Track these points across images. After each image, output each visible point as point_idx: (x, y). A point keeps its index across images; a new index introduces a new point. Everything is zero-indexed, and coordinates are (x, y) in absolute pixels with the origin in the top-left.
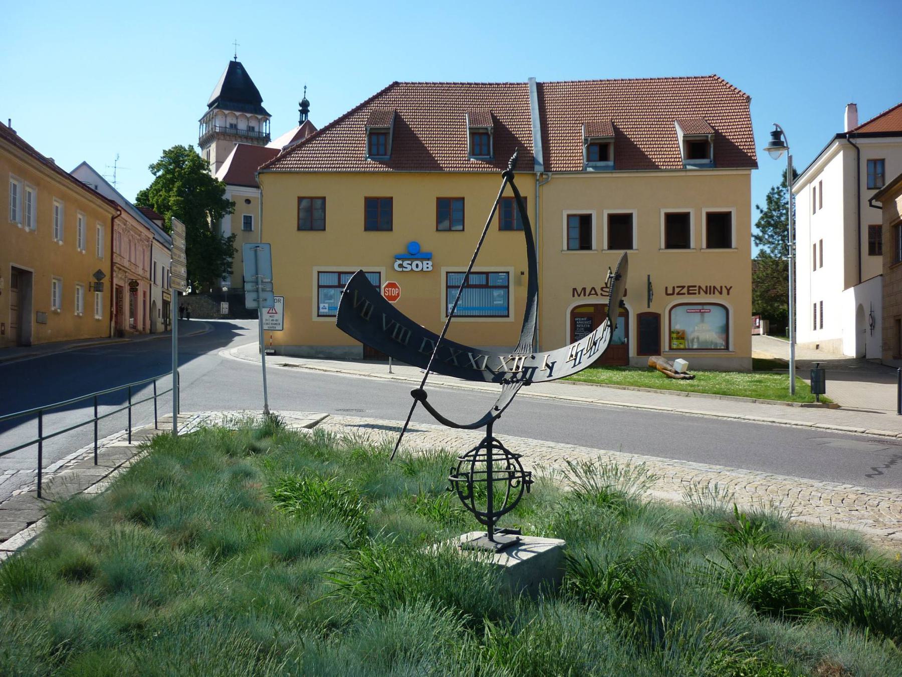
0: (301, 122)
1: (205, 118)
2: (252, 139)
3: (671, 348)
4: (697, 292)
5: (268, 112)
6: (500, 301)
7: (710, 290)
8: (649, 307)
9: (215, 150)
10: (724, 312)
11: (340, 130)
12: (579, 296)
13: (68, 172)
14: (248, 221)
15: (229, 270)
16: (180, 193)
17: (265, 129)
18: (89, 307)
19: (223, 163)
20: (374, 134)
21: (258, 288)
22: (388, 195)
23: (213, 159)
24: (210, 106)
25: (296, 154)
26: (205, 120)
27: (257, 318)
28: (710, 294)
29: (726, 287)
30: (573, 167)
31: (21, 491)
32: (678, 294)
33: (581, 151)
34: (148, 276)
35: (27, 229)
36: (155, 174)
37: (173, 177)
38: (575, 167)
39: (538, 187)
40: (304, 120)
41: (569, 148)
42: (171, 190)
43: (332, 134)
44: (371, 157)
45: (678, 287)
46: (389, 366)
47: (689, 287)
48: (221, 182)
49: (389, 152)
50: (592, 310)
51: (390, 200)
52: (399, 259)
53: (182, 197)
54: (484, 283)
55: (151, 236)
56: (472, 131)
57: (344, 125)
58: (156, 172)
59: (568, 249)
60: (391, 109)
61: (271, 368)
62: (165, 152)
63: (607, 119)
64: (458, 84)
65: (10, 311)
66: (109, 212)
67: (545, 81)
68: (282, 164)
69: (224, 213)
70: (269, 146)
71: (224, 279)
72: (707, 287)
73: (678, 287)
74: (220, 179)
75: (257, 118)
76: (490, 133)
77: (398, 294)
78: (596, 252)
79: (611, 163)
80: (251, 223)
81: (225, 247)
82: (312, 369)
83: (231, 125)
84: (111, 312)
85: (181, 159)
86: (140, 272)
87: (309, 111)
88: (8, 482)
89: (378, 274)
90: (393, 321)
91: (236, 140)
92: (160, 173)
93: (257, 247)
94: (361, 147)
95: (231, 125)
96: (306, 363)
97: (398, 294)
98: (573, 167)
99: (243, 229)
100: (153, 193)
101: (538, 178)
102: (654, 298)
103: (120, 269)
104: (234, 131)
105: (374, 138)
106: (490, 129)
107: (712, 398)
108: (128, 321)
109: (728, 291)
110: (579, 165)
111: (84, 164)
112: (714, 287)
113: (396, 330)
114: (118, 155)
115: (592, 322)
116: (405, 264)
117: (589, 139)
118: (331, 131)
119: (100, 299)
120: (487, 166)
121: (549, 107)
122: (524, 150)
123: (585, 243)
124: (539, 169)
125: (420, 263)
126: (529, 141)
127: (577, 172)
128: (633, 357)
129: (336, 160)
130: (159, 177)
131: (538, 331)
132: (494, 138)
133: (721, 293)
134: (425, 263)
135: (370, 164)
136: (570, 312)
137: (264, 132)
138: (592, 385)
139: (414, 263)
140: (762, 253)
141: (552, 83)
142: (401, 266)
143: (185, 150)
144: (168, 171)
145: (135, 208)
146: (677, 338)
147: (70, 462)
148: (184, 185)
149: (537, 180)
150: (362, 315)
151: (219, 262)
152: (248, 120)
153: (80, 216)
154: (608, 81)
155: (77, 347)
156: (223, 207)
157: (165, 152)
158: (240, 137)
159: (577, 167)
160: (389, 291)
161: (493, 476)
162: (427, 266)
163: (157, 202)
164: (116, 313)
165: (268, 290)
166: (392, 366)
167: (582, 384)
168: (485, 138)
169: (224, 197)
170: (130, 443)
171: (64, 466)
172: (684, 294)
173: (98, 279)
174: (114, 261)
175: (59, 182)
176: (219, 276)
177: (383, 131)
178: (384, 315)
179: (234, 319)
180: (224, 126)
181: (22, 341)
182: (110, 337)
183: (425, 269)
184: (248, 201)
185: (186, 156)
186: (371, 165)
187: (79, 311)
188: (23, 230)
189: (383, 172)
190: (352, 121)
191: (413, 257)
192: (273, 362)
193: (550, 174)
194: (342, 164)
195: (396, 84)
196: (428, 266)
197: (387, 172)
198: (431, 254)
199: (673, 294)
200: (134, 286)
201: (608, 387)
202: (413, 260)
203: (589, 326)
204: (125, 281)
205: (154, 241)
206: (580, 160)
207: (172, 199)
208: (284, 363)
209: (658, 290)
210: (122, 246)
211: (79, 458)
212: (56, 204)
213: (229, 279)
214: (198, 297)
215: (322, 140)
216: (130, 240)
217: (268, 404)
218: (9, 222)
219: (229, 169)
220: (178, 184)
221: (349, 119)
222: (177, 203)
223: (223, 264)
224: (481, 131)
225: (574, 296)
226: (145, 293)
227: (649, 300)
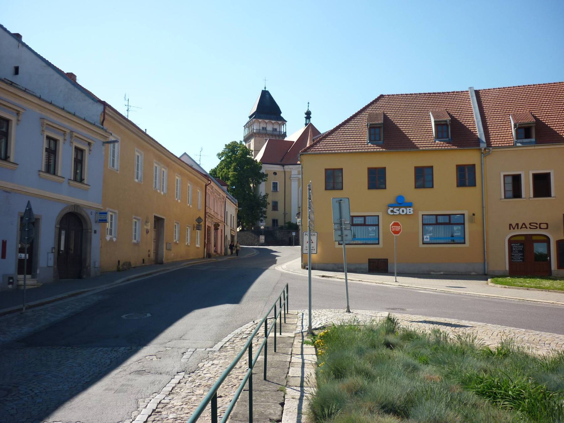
0: (306, 124)
1: (247, 125)
2: (275, 136)
5: (285, 119)
9: (253, 143)
11: (349, 126)
12: (514, 229)
14: (275, 185)
15: (264, 215)
16: (235, 170)
17: (283, 129)
18: (193, 239)
19: (259, 151)
20: (372, 128)
21: (342, 228)
22: (383, 166)
23: (252, 148)
24: (250, 117)
25: (323, 142)
26: (248, 126)
27: (297, 244)
30: (506, 143)
31: (203, 364)
33: (511, 133)
34: (224, 221)
35: (162, 193)
36: (220, 159)
37: (230, 160)
38: (508, 143)
39: (483, 157)
40: (308, 123)
41: (502, 131)
42: (230, 168)
43: (344, 128)
44: (371, 142)
46: (394, 277)
48: (259, 162)
49: (382, 139)
50: (523, 238)
51: (383, 170)
52: (391, 207)
53: (236, 172)
54: (363, 223)
55: (225, 196)
56: (437, 123)
57: (351, 123)
58: (221, 158)
59: (505, 198)
60: (381, 111)
61: (314, 278)
62: (226, 145)
63: (527, 111)
64: (422, 94)
65: (153, 242)
66: (204, 182)
67: (480, 89)
68: (314, 149)
69: (261, 181)
70: (286, 139)
71: (262, 221)
74: (258, 161)
75: (278, 123)
76: (448, 123)
77: (400, 230)
78: (525, 199)
79: (533, 140)
80: (277, 187)
81: (262, 202)
82: (342, 279)
83: (263, 128)
84: (205, 242)
85: (236, 149)
86: (220, 218)
87: (311, 117)
88: (192, 357)
89: (463, 215)
91: (266, 137)
92: (223, 158)
93: (340, 200)
94: (364, 136)
95: (263, 128)
96: (336, 275)
97: (400, 230)
98: (506, 143)
100: (219, 170)
101: (483, 151)
103: (209, 216)
104: (264, 132)
105: (372, 130)
106: (448, 121)
108: (213, 249)
110: (510, 142)
114: (202, 148)
115: (523, 247)
116: (395, 210)
117: (518, 124)
118: (343, 127)
119: (199, 234)
120: (448, 145)
121: (485, 105)
122: (471, 134)
123: (517, 193)
124: (483, 146)
125: (404, 209)
126: (474, 128)
127: (509, 147)
128: (555, 270)
129: (348, 145)
130: (223, 160)
131: (486, 253)
132: (451, 127)
134: (408, 209)
135: (370, 147)
136: (507, 240)
137: (283, 131)
138: (542, 291)
139: (401, 209)
141: (485, 90)
142: (392, 211)
143: (238, 144)
144: (228, 157)
147: (226, 343)
148: (237, 165)
149: (482, 153)
151: (259, 211)
152: (273, 125)
153: (189, 185)
154: (484, 90)
155: (189, 264)
156: (260, 177)
157: (226, 145)
158: (268, 135)
159: (510, 143)
160: (394, 228)
162: (410, 211)
163: (222, 175)
164: (207, 244)
165: (348, 229)
166: (397, 277)
167: (534, 290)
168: (445, 127)
169: (261, 171)
170: (281, 334)
171: (223, 347)
173: (198, 223)
174: (207, 211)
175: (180, 165)
176: (258, 219)
177: (378, 126)
179: (269, 246)
180: (259, 129)
181: (158, 262)
182: (204, 258)
183: (408, 213)
184: (275, 173)
185: (238, 147)
186: (372, 147)
187: (188, 242)
188: (160, 193)
189: (379, 152)
190: (356, 120)
191: (400, 205)
192: (315, 274)
193: (491, 148)
194: (323, 148)
195: (382, 96)
196: (410, 211)
197: (382, 151)
198: (411, 203)
200: (216, 226)
201: (555, 292)
202: (400, 207)
203: (521, 249)
204: (212, 223)
205: (227, 199)
206: (511, 138)
207: (231, 173)
208: (322, 275)
210: (210, 202)
211: (230, 341)
212: (177, 178)
213: (264, 221)
214: (246, 233)
215: (338, 133)
216: (214, 199)
217: (349, 305)
218: (153, 189)
219: (264, 154)
220: (234, 164)
221: (354, 119)
222: (234, 176)
223: (261, 212)
224: (443, 123)
225: (510, 229)
226: (222, 230)
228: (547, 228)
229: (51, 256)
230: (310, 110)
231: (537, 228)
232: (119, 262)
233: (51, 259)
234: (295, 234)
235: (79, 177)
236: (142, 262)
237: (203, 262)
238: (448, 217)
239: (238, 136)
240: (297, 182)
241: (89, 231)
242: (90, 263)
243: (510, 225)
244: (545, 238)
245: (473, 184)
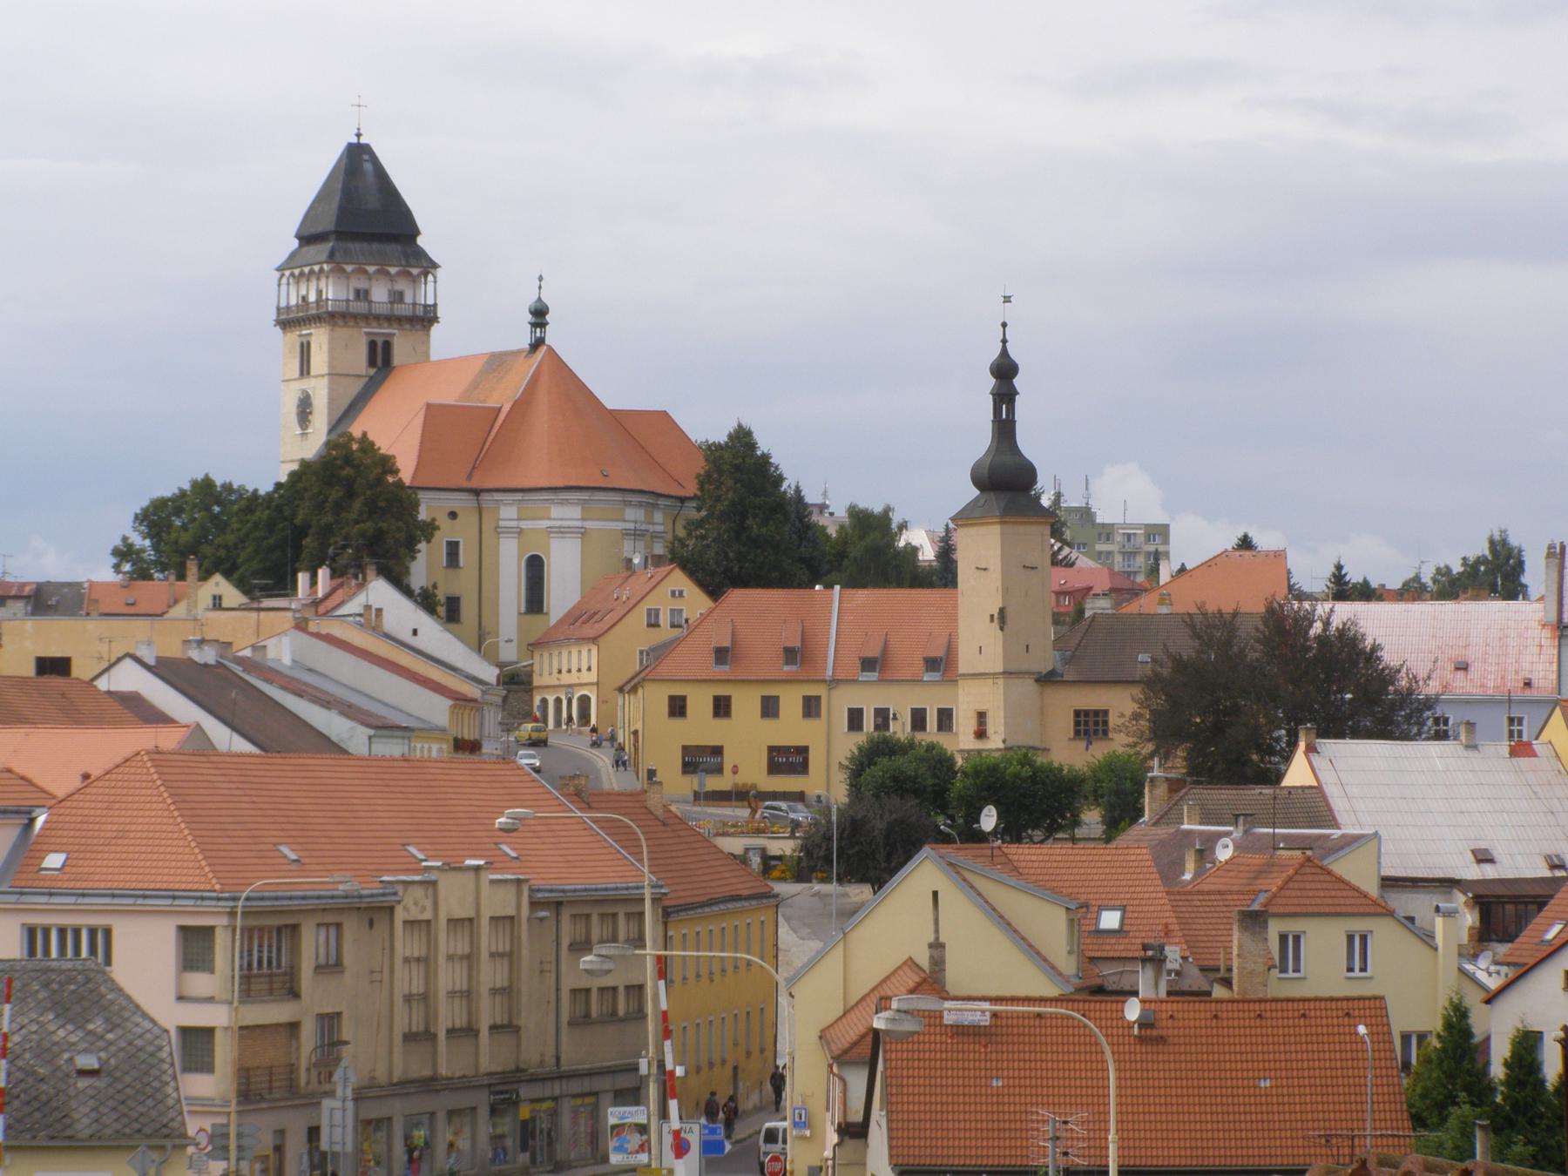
6: (418, 988)
99: (445, 564)
145: (1403, 920)
158: (377, 318)
161: (643, 514)
236: (375, 922)
237: (273, 906)
239: (400, 475)
240: (516, 540)
245: (818, 715)
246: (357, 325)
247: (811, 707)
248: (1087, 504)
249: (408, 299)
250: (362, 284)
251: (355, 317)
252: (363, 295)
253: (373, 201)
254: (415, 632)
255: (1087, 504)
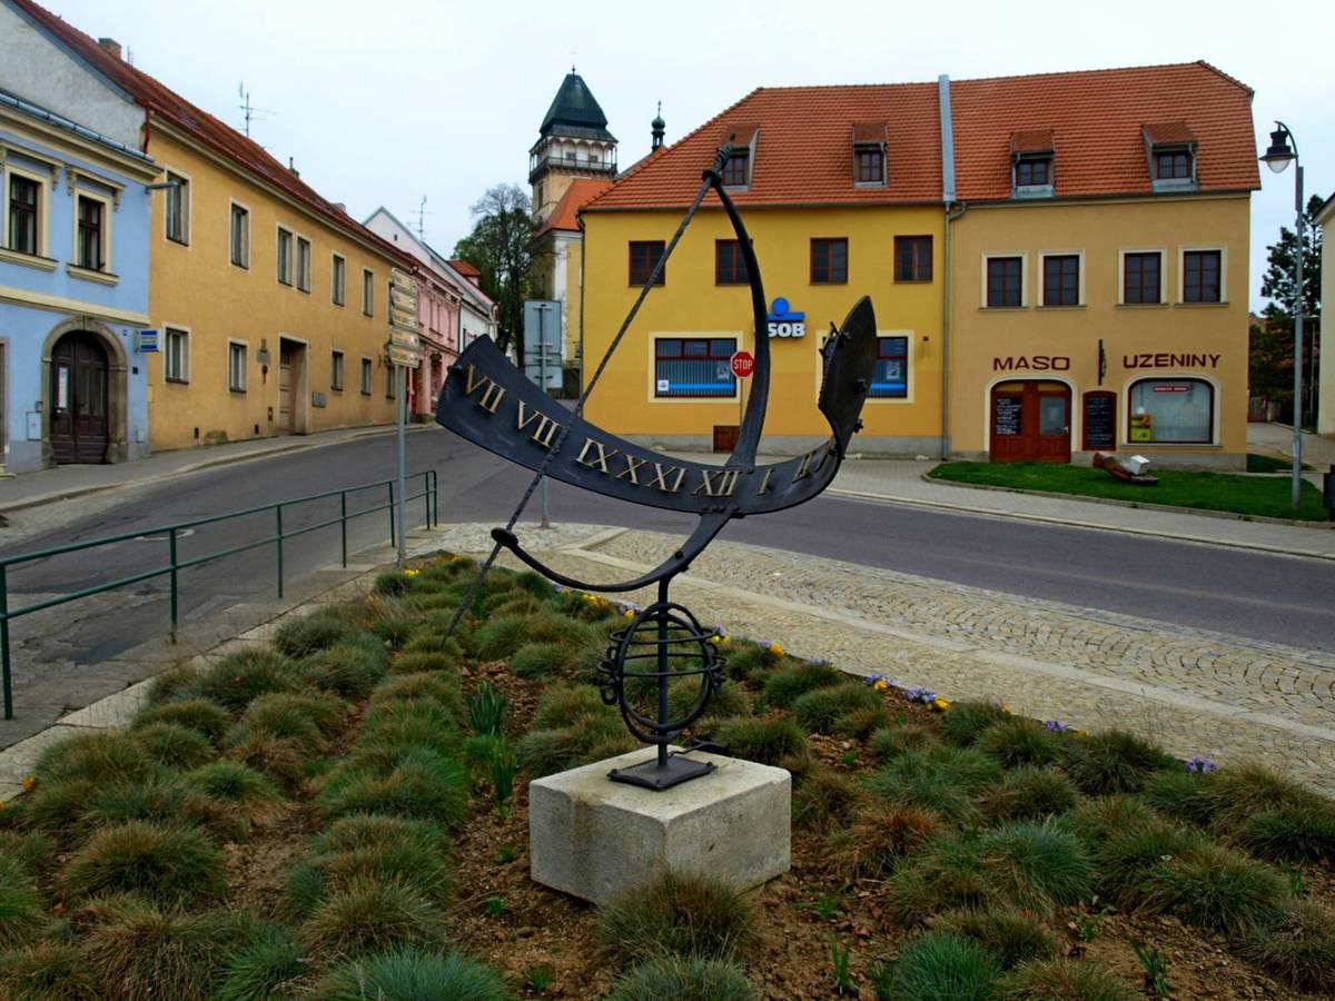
3: (1129, 441)
4: (1169, 363)
7: (1188, 360)
8: (1100, 383)
10: (1207, 390)
12: (1003, 368)
13: (360, 222)
21: (541, 361)
26: (539, 150)
28: (1188, 365)
29: (1211, 356)
32: (1142, 366)
45: (1142, 356)
47: (1157, 356)
50: (1020, 388)
72: (1183, 356)
73: (1142, 356)
86: (445, 342)
87: (663, 134)
90: (538, 413)
102: (1107, 372)
107: (1177, 512)
109: (1214, 361)
111: (382, 210)
112: (1194, 357)
113: (541, 427)
128: (1076, 453)
133: (1203, 364)
134: (795, 325)
139: (781, 326)
140: (1271, 309)
146: (1139, 427)
150: (483, 403)
158: (580, 170)
170: (345, 566)
172: (1150, 366)
178: (522, 404)
183: (795, 334)
195: (761, 89)
198: (802, 314)
199: (1135, 366)
202: (779, 322)
209: (1113, 361)
225: (995, 368)
227: (1101, 375)
228: (1067, 368)
229: (37, 419)
230: (662, 117)
231: (1047, 367)
232: (197, 431)
233: (34, 425)
234: (666, 382)
235: (91, 259)
238: (705, 345)
241: (121, 368)
242: (126, 433)
243: (997, 360)
244: (1062, 389)
246: (567, 174)
247: (912, 260)
248: (1159, 161)
249: (600, 160)
250: (572, 151)
251: (566, 169)
252: (571, 157)
253: (579, 104)
254: (396, 238)
255: (1159, 161)
